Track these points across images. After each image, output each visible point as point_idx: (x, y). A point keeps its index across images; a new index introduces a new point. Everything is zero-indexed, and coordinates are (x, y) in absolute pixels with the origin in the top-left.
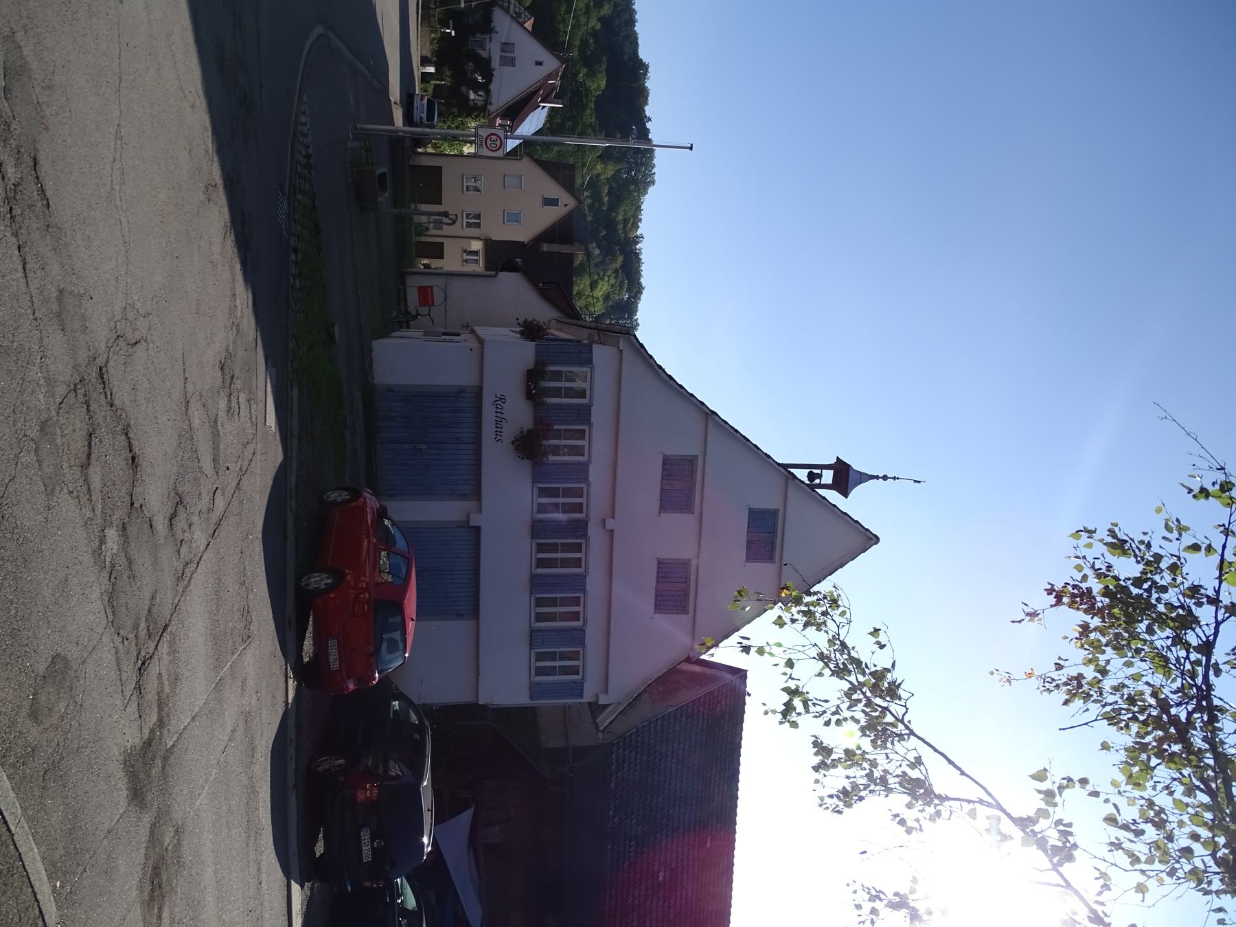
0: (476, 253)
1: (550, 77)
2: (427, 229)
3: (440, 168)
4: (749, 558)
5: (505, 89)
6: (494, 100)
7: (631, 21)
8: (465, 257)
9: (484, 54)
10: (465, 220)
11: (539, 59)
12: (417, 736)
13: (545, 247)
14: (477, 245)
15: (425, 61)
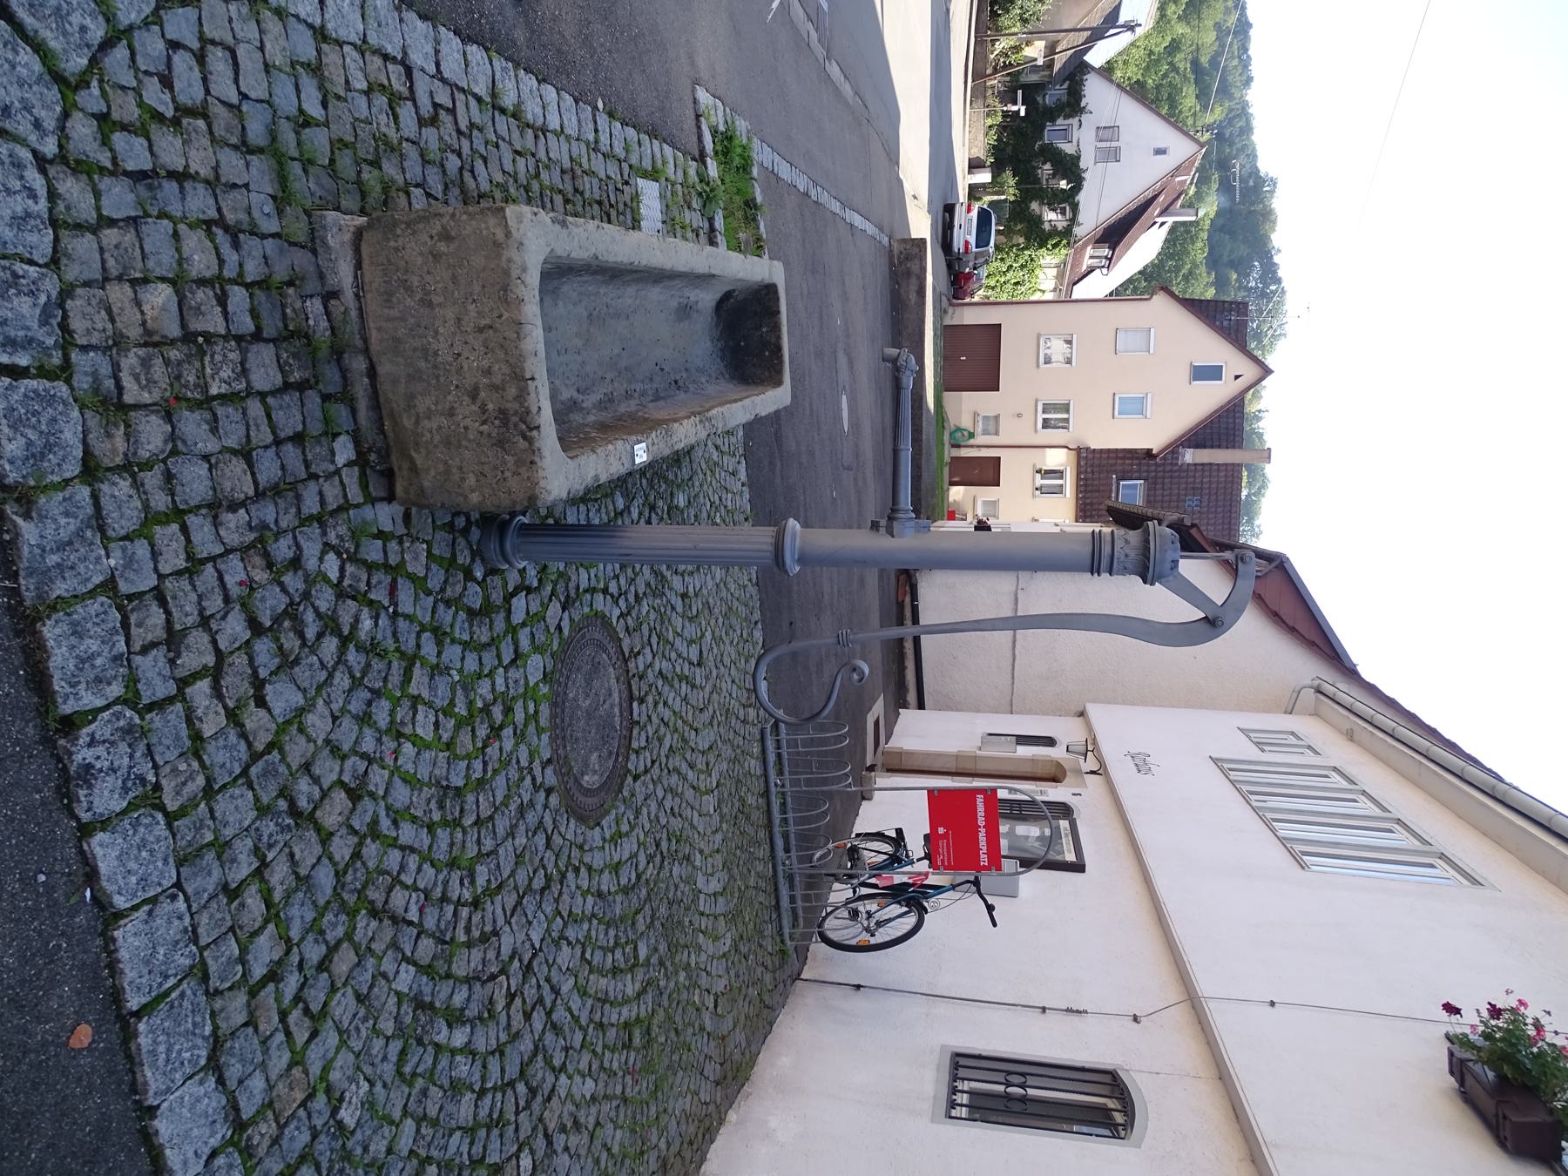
0: (1059, 474)
1: (1178, 170)
2: (972, 435)
3: (997, 328)
4: (995, 387)
5: (1100, 201)
6: (1081, 218)
7: (1247, 129)
8: (1039, 481)
9: (1069, 149)
10: (1041, 416)
11: (1162, 146)
12: (941, 831)
13: (1189, 456)
14: (1057, 459)
15: (975, 165)
